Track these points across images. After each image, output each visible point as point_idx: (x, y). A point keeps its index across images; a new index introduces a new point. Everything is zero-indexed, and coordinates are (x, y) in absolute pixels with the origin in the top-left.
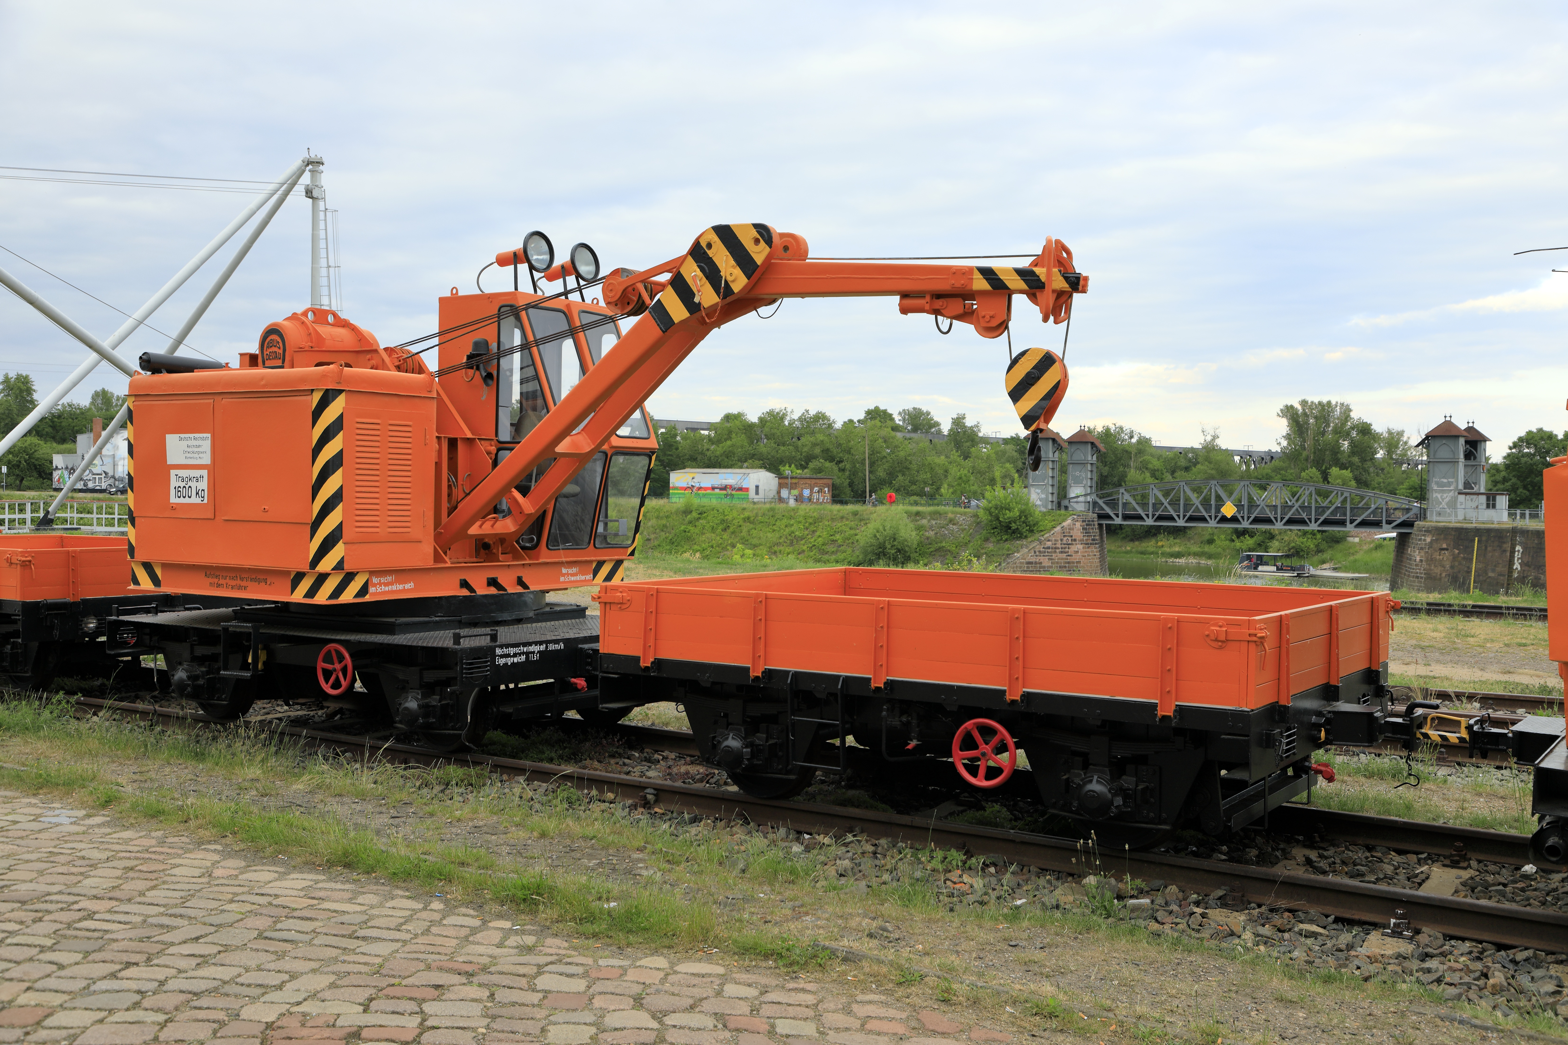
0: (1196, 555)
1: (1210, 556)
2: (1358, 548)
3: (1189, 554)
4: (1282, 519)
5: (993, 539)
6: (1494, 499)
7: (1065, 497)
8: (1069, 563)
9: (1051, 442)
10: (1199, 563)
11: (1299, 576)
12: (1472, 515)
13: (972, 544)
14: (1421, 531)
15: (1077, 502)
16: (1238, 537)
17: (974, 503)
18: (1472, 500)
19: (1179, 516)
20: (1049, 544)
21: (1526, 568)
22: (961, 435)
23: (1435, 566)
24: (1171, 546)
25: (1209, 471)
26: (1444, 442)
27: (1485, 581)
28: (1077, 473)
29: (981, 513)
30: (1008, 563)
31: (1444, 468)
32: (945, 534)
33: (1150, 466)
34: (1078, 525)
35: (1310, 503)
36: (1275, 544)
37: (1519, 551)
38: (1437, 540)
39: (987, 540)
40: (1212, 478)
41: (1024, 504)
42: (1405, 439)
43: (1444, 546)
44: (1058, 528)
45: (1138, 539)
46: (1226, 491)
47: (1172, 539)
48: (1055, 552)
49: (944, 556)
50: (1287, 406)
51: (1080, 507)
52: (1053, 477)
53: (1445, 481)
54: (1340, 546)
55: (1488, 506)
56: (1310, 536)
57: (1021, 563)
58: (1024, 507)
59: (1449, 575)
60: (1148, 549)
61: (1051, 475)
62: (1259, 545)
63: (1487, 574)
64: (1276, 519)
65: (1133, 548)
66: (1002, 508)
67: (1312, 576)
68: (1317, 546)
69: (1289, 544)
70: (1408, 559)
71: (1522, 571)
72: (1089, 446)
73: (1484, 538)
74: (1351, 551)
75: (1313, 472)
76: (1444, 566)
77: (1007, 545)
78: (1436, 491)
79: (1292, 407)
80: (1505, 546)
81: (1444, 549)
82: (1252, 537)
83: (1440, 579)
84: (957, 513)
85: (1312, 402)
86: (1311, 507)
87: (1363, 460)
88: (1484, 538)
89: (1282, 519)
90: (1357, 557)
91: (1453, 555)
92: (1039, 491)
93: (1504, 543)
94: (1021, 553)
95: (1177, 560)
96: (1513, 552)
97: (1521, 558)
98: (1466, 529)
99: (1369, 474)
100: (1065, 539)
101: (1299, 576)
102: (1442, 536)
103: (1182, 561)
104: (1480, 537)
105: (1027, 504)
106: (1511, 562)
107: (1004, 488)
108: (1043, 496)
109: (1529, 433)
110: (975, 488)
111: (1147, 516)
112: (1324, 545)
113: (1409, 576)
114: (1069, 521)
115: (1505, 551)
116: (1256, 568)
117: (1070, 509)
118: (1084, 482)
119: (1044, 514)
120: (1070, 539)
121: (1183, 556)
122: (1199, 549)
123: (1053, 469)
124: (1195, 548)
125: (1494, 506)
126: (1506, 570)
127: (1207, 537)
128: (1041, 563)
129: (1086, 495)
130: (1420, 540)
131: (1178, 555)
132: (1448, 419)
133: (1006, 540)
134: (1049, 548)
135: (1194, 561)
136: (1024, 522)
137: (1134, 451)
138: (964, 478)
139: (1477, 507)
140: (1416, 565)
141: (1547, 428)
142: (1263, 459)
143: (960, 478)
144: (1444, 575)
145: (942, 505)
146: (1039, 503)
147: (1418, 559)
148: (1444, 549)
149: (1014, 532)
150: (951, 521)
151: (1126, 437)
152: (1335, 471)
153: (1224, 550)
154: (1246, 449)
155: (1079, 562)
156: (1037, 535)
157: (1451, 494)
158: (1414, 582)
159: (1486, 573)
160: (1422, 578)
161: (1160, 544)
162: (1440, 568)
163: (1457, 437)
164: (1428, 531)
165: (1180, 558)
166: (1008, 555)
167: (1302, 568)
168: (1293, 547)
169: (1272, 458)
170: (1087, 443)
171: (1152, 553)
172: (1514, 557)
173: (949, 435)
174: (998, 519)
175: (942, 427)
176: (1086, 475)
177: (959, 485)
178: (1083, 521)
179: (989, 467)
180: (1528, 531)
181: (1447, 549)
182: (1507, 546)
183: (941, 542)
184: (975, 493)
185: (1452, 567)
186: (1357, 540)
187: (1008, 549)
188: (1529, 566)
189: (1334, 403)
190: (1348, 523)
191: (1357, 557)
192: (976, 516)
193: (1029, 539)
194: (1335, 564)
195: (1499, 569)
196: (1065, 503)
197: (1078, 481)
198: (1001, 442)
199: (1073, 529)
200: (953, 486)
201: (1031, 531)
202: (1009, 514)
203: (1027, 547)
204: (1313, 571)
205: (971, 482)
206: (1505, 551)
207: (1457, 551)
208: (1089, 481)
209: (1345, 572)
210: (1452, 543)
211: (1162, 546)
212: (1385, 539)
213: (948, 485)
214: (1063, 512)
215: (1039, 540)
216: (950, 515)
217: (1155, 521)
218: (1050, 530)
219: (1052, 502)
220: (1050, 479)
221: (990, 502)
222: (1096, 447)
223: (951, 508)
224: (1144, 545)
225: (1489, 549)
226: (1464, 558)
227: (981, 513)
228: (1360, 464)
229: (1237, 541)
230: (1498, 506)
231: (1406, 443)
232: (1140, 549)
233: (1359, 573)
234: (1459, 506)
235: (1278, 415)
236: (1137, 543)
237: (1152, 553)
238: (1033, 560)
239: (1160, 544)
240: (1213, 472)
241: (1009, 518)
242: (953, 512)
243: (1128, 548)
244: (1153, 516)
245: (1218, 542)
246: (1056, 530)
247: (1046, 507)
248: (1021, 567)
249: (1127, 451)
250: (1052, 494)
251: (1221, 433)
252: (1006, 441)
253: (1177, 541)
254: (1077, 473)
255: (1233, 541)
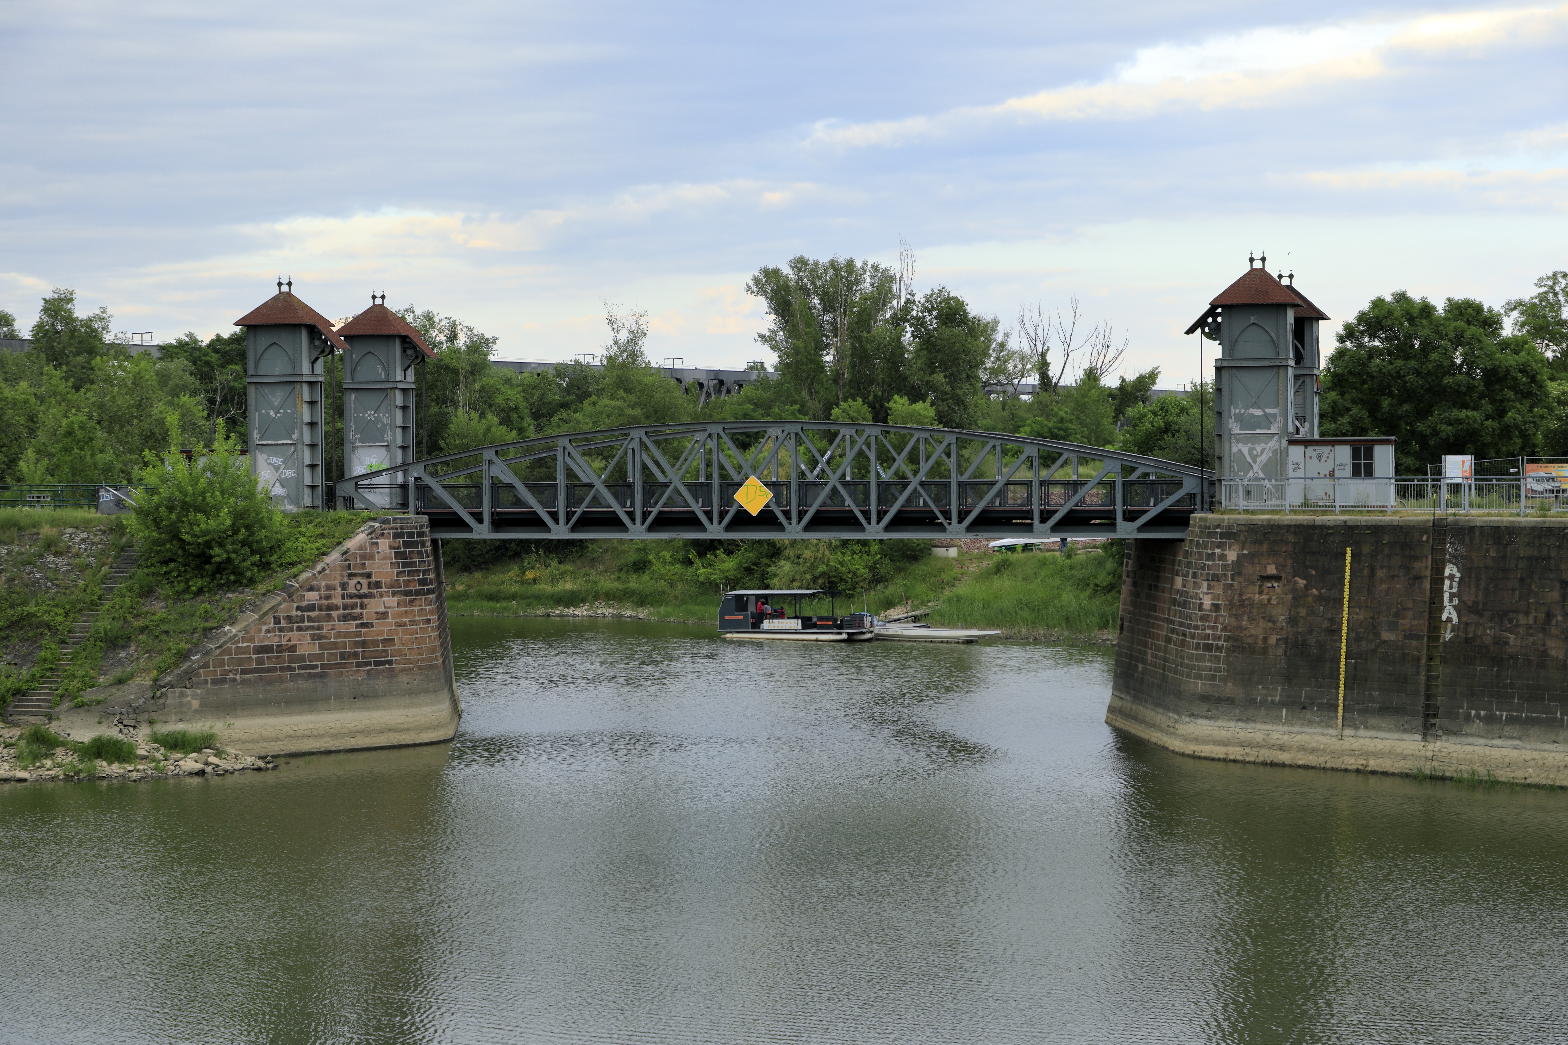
0: (610, 597)
1: (642, 600)
2: (957, 570)
3: (596, 597)
4: (881, 515)
5: (164, 590)
6: (1370, 455)
7: (341, 476)
8: (364, 644)
9: (304, 335)
10: (620, 616)
11: (851, 640)
12: (1319, 490)
13: (108, 605)
14: (1211, 535)
15: (371, 487)
16: (701, 555)
17: (107, 495)
18: (1319, 458)
19: (631, 515)
20: (312, 597)
21: (1472, 618)
22: (65, 338)
23: (1251, 619)
24: (553, 580)
25: (629, 411)
26: (1253, 319)
27: (1374, 651)
28: (370, 415)
29: (130, 520)
30: (208, 653)
31: (1254, 382)
32: (35, 582)
33: (499, 400)
34: (384, 544)
35: (709, 476)
36: (785, 567)
37: (1452, 577)
38: (1252, 556)
39: (147, 592)
40: (634, 423)
41: (244, 497)
42: (999, 337)
43: (1272, 570)
44: (334, 556)
45: (479, 567)
46: (665, 452)
47: (555, 563)
48: (329, 618)
49: (34, 640)
50: (766, 272)
51: (382, 499)
52: (312, 425)
53: (1258, 412)
54: (919, 568)
55: (1356, 472)
56: (857, 548)
57: (239, 650)
58: (243, 504)
59: (1286, 641)
60: (504, 587)
61: (307, 418)
62: (749, 570)
63: (1377, 635)
64: (867, 514)
65: (469, 587)
66: (186, 507)
67: (879, 638)
68: (872, 568)
69: (813, 567)
70: (1174, 602)
71: (1464, 625)
72: (398, 346)
73: (1366, 549)
74: (945, 577)
75: (858, 406)
76: (1271, 619)
77: (203, 605)
78: (1239, 438)
79: (776, 272)
80: (1417, 565)
81: (1270, 578)
82: (729, 553)
83: (1265, 651)
84: (66, 524)
85: (816, 264)
86: (708, 485)
87: (953, 379)
88: (1366, 549)
89: (881, 515)
90: (961, 589)
91: (1294, 590)
92: (277, 461)
93: (1416, 558)
94: (241, 625)
95: (571, 611)
96: (1438, 579)
97: (1458, 595)
98: (1323, 527)
99: (966, 408)
100: (353, 582)
101: (851, 640)
102: (1265, 547)
103: (582, 612)
104: (1357, 548)
105: (251, 495)
106: (1435, 605)
107: (189, 456)
108: (290, 473)
109: (1378, 303)
110: (107, 457)
111: (554, 516)
112: (886, 568)
113: (1183, 644)
114: (361, 538)
115: (1418, 578)
116: (756, 625)
117: (357, 504)
118: (388, 436)
119: (296, 520)
120: (365, 582)
121: (583, 601)
122: (616, 584)
123: (312, 403)
124: (608, 583)
125: (1369, 472)
126: (1422, 624)
127: (633, 557)
128: (293, 648)
129: (394, 469)
130: (1211, 557)
131: (572, 599)
132: (1258, 264)
133: (200, 591)
134: (311, 608)
135: (608, 611)
136: (244, 543)
137: (463, 367)
138: (79, 434)
139: (1332, 474)
140: (1204, 618)
141: (1416, 295)
142: (701, 385)
143: (69, 433)
144: (1273, 640)
145: (25, 503)
146: (278, 491)
147: (1207, 602)
148: (1270, 578)
149: (220, 569)
150: (50, 545)
151: (442, 338)
152: (899, 404)
153: (672, 584)
154: (669, 365)
155: (390, 641)
156: (280, 577)
157: (1273, 443)
158: (1201, 658)
159: (1374, 630)
160: (1219, 649)
161: (530, 575)
162: (1262, 624)
163: (1280, 307)
164: (1230, 534)
165: (576, 606)
166: (207, 631)
167: (856, 621)
168: (823, 574)
169: (721, 382)
170: (390, 337)
171: (514, 597)
172: (1442, 592)
173: (36, 339)
174: (175, 536)
175: (17, 325)
176: (393, 419)
177: (67, 450)
178: (397, 536)
179: (139, 406)
180: (1472, 529)
181: (1277, 578)
182: (1424, 567)
183: (24, 603)
184: (107, 469)
185: (1293, 621)
186: (953, 552)
187: (207, 616)
188: (1479, 613)
189: (859, 264)
190: (1036, 521)
191: (961, 589)
192: (118, 529)
193: (261, 588)
194: (916, 608)
195: (1405, 622)
196: (344, 489)
197: (372, 436)
198: (156, 354)
199: (371, 557)
200: (50, 455)
201: (265, 565)
202: (206, 524)
203: (255, 608)
204: (881, 629)
205: (97, 444)
206: (1418, 578)
207: (1302, 582)
208: (399, 432)
209: (943, 625)
210: (1289, 562)
211: (535, 581)
212: (1011, 548)
213: (38, 452)
214: (342, 513)
215: (286, 588)
216: (47, 531)
217: (573, 529)
218: (315, 561)
219: (313, 487)
220: (306, 430)
221: (152, 491)
222: (414, 347)
223: (48, 511)
224: (494, 578)
225: (1380, 573)
226: (1320, 599)
227: (130, 520)
228: (948, 389)
229: (698, 563)
230: (1377, 471)
231: (1002, 346)
232: (486, 588)
233: (967, 626)
234: (1291, 474)
235: (749, 289)
236: (478, 575)
237: (514, 597)
238: (273, 640)
239: (530, 575)
240: (637, 412)
241: (205, 533)
242: (53, 523)
243: (460, 588)
244: (569, 515)
245: (657, 566)
246: (328, 559)
247: (297, 502)
248: (240, 662)
249: (447, 368)
250: (313, 467)
251: (653, 325)
252: (167, 352)
253: (568, 567)
254: (370, 415)
255: (690, 563)
